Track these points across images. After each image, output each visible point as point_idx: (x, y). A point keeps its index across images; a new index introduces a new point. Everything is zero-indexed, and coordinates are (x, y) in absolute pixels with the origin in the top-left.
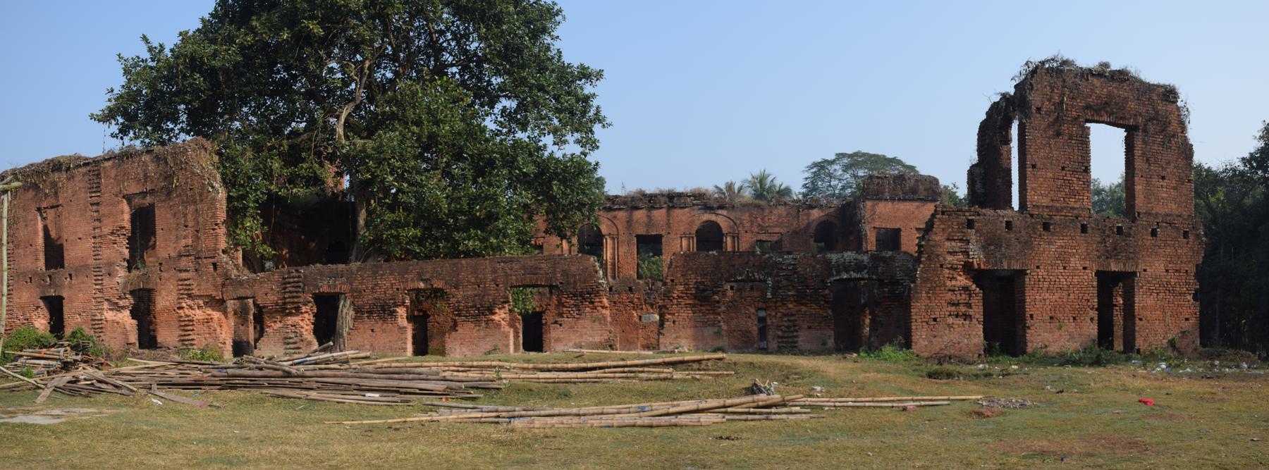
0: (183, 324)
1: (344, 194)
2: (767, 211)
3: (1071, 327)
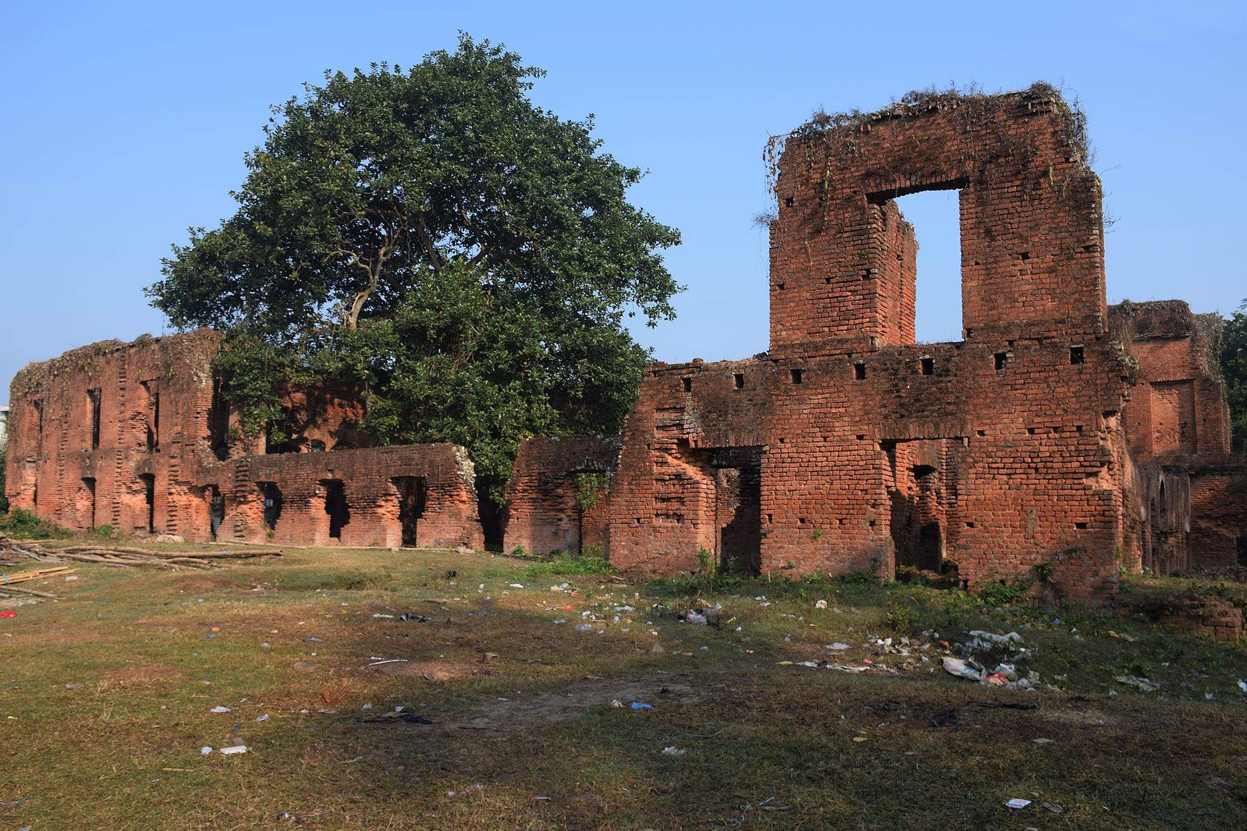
0: (170, 509)
3: (833, 534)
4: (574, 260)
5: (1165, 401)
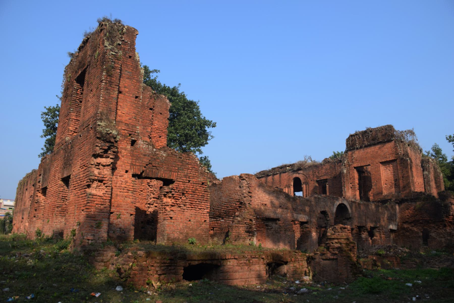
1: (444, 191)
2: (320, 168)
4: (150, 145)
5: (387, 170)
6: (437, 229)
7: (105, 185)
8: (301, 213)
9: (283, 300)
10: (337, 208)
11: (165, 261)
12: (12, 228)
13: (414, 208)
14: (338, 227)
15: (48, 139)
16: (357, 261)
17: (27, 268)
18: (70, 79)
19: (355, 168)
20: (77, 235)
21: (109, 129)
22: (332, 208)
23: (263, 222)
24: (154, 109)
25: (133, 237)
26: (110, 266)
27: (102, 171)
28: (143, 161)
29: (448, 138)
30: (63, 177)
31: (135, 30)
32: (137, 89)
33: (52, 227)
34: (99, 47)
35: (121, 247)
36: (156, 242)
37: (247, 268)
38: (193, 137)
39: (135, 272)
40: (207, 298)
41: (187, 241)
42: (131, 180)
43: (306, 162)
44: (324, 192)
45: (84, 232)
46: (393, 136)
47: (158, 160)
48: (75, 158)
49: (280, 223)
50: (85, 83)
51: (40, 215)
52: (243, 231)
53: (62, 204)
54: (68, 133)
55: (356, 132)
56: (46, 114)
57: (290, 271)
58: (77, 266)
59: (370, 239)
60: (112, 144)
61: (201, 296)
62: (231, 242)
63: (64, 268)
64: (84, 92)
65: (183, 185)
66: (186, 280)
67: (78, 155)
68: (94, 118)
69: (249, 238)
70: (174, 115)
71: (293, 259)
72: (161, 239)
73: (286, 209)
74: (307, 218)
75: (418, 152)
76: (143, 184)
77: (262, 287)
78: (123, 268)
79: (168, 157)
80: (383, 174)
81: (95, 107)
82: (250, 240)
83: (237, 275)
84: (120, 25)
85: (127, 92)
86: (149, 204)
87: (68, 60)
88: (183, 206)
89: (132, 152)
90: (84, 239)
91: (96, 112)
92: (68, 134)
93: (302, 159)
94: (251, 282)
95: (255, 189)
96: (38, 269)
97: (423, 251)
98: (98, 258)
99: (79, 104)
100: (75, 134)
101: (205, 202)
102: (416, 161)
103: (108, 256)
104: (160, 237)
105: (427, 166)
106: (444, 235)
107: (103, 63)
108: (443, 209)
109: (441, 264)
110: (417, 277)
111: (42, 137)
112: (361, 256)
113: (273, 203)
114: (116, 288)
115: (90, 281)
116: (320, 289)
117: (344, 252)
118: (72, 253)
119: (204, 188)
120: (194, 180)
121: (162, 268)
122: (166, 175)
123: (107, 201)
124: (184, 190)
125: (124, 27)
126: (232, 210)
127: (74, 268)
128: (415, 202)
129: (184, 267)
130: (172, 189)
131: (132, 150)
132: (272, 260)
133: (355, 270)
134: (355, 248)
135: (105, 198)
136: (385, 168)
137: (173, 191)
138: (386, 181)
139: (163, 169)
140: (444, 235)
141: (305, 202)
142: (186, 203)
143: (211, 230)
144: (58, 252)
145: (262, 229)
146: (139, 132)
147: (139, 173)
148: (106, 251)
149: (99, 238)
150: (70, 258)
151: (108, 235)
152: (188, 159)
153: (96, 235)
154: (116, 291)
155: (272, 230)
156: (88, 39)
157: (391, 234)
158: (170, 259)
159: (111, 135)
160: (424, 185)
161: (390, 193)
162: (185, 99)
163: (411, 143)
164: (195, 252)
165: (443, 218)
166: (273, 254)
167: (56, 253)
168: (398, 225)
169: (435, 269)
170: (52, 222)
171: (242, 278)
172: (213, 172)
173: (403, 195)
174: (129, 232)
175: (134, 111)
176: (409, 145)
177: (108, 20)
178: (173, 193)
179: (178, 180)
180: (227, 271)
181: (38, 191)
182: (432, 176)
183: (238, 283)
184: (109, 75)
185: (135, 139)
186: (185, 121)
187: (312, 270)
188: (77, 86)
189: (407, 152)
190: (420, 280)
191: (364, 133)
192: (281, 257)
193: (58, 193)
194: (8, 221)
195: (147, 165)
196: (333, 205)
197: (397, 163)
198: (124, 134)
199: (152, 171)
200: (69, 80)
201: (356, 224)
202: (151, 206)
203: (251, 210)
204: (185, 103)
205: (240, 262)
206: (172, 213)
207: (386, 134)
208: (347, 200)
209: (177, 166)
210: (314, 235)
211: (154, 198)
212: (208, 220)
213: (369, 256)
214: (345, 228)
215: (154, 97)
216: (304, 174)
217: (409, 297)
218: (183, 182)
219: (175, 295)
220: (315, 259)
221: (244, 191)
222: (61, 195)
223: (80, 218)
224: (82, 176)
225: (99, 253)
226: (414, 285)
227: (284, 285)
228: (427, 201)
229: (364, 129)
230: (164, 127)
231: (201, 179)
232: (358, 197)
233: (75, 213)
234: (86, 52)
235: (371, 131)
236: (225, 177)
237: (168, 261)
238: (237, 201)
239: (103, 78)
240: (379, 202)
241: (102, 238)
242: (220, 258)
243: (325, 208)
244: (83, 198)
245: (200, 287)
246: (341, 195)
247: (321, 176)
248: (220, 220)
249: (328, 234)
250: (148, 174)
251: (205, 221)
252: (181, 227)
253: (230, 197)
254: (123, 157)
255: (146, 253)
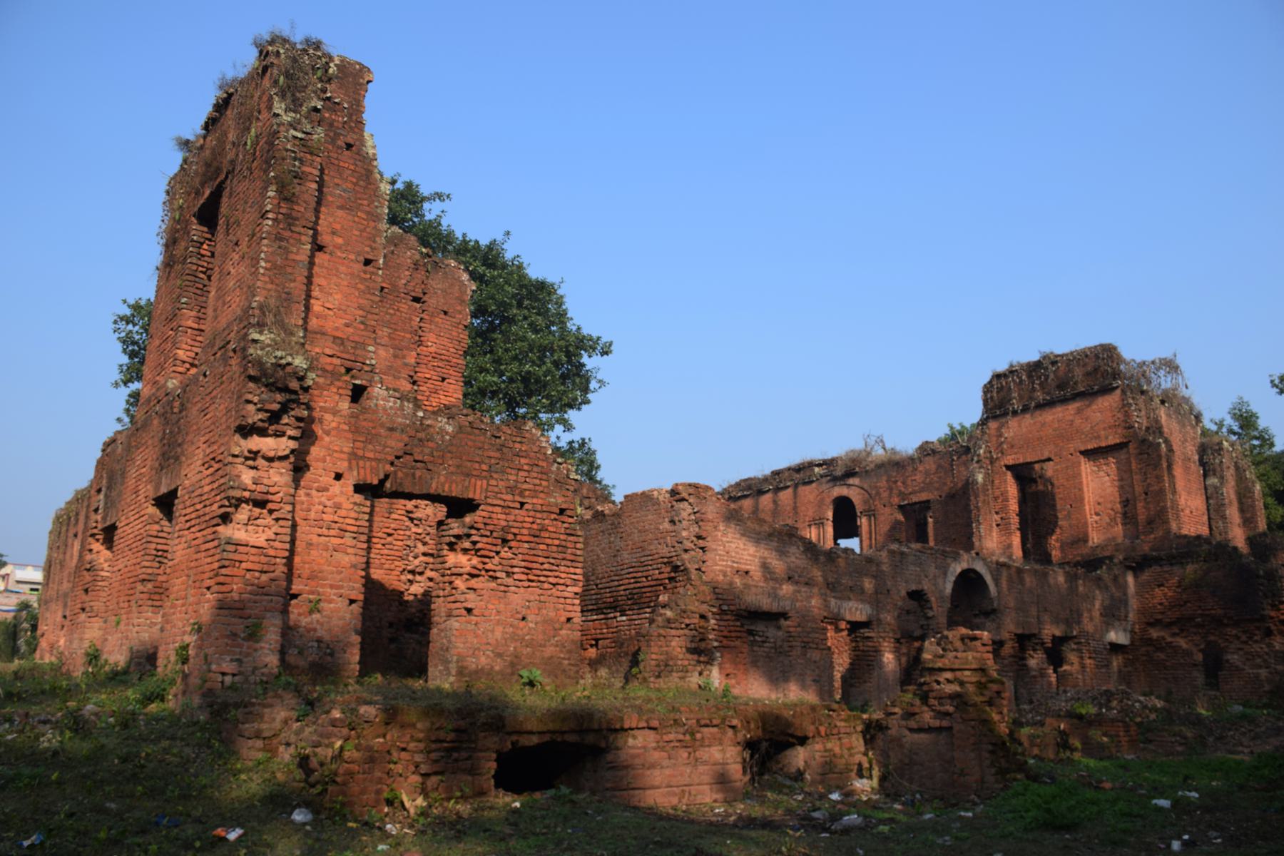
1: (1264, 534)
2: (910, 469)
4: (408, 401)
5: (1102, 474)
6: (1246, 643)
7: (274, 516)
8: (851, 596)
9: (784, 849)
10: (956, 582)
11: (442, 735)
12: (36, 645)
13: (1179, 582)
14: (954, 636)
15: (134, 392)
16: (1011, 734)
17: (34, 757)
18: (181, 215)
19: (1008, 467)
20: (191, 660)
21: (284, 353)
22: (940, 581)
23: (738, 624)
24: (425, 298)
25: (358, 667)
26: (282, 748)
27: (265, 475)
28: (385, 447)
29: (1277, 382)
30: (159, 494)
31: (363, 69)
32: (370, 238)
33: (127, 638)
34: (258, 119)
35: (315, 695)
36: (426, 681)
37: (686, 755)
38: (545, 385)
39: (351, 766)
40: (558, 843)
41: (516, 677)
42: (352, 500)
43: (869, 454)
44: (921, 536)
45: (211, 651)
46: (1116, 375)
47: (430, 444)
48: (189, 438)
49: (789, 627)
50: (221, 222)
51: (98, 605)
52: (679, 650)
53: (156, 571)
54: (174, 368)
55: (1012, 366)
56: (128, 320)
57: (813, 763)
58: (187, 750)
59: (1051, 671)
60: (293, 397)
61: (542, 838)
62: (645, 679)
63: (148, 754)
64: (219, 249)
65: (504, 516)
66: (507, 790)
67: (199, 429)
68: (241, 321)
69: (699, 669)
70: (492, 323)
71: (822, 729)
72: (440, 671)
73: (807, 584)
74: (869, 611)
75: (1190, 421)
76: (394, 516)
77: (730, 811)
78: (315, 755)
79: (460, 436)
80: (1088, 484)
81: (245, 289)
82: (700, 674)
83: (656, 776)
84: (319, 53)
85: (339, 247)
86: (412, 572)
87: (173, 161)
88: (504, 575)
89: (353, 420)
90: (210, 671)
91: (247, 304)
92: (174, 371)
93: (859, 445)
94: (699, 797)
95: (715, 527)
96: (70, 759)
97: (1205, 705)
98: (247, 726)
99: (205, 286)
100: (193, 371)
101: (569, 563)
102: (1185, 448)
103: (274, 719)
104: (436, 666)
105: (1217, 461)
106: (1265, 661)
107: (267, 162)
108: (1262, 585)
109: (1259, 742)
110: (1186, 782)
111: (116, 385)
112: (1024, 720)
113: (768, 568)
114: (291, 813)
115: (217, 794)
116: (901, 817)
117: (971, 709)
118: (177, 712)
119: (565, 525)
120: (535, 501)
121: (434, 756)
122: (454, 485)
123: (278, 560)
124: (505, 529)
125: (331, 59)
126: (650, 589)
127: (174, 755)
128: (1182, 563)
129: (497, 752)
130: (472, 527)
131: (352, 416)
132: (760, 733)
133: (1003, 761)
134: (1003, 695)
135: (272, 552)
136: (1096, 469)
137: (473, 532)
138: (1099, 504)
139: (445, 469)
140: (1265, 661)
141: (865, 564)
142: (512, 567)
143: (592, 646)
144: (138, 711)
145: (738, 643)
146: (374, 362)
147: (375, 482)
148: (271, 706)
149: (255, 669)
150: (170, 727)
151: (283, 660)
152: (519, 439)
153: (245, 660)
154: (293, 822)
155: (767, 644)
156: (230, 95)
157: (1114, 658)
158: (455, 730)
159: (288, 369)
160: (1209, 515)
161: (1109, 539)
162: (523, 277)
163: (1168, 397)
164: (532, 710)
165: (1263, 609)
166: (764, 713)
167: (133, 713)
168: (1132, 632)
169: (1238, 757)
170: (127, 624)
171: (672, 784)
172: (604, 483)
173: (1145, 546)
174: (345, 652)
175: (361, 301)
176: (1163, 402)
177: (285, 41)
178: (475, 538)
179: (489, 501)
180: (625, 764)
181: (93, 535)
182: (1229, 491)
183: (658, 801)
184: (286, 197)
185: (364, 383)
186: (524, 339)
187: (879, 762)
188: (200, 233)
189: (1157, 421)
190: (1196, 790)
191: (1034, 369)
192: (788, 724)
193: (144, 540)
194: (26, 625)
195: (398, 457)
196: (945, 574)
197: (1128, 452)
198: (329, 368)
199: (413, 475)
200: (177, 217)
201: (1012, 627)
202: (418, 578)
203: (705, 587)
204: (521, 287)
205: (666, 738)
206: (471, 595)
207: (1096, 370)
208: (984, 560)
209: (487, 461)
210: (888, 658)
211: (425, 554)
212: (578, 618)
213: (1048, 720)
214: (974, 639)
215: (425, 264)
216: (862, 488)
217: (1160, 839)
218: (503, 507)
219: (465, 834)
220: (887, 728)
221: (684, 534)
222: (153, 546)
223: (202, 611)
224: (207, 489)
225: (251, 713)
226: (1176, 803)
227: (795, 804)
228: (1216, 560)
229: (1035, 357)
230: (454, 351)
231: (558, 499)
232: (1017, 552)
233: (189, 596)
234: (225, 134)
235: (1054, 363)
236: (629, 492)
237: (451, 736)
238: (665, 564)
239: (269, 207)
240: (1077, 564)
241: (264, 670)
242: (604, 726)
243: (920, 583)
244: (211, 552)
245: (544, 813)
246: (969, 546)
247: (910, 493)
248: (615, 617)
249: (926, 656)
250: (401, 484)
251: (569, 620)
252: (499, 638)
253: (643, 551)
254: (328, 433)
255: (386, 711)
